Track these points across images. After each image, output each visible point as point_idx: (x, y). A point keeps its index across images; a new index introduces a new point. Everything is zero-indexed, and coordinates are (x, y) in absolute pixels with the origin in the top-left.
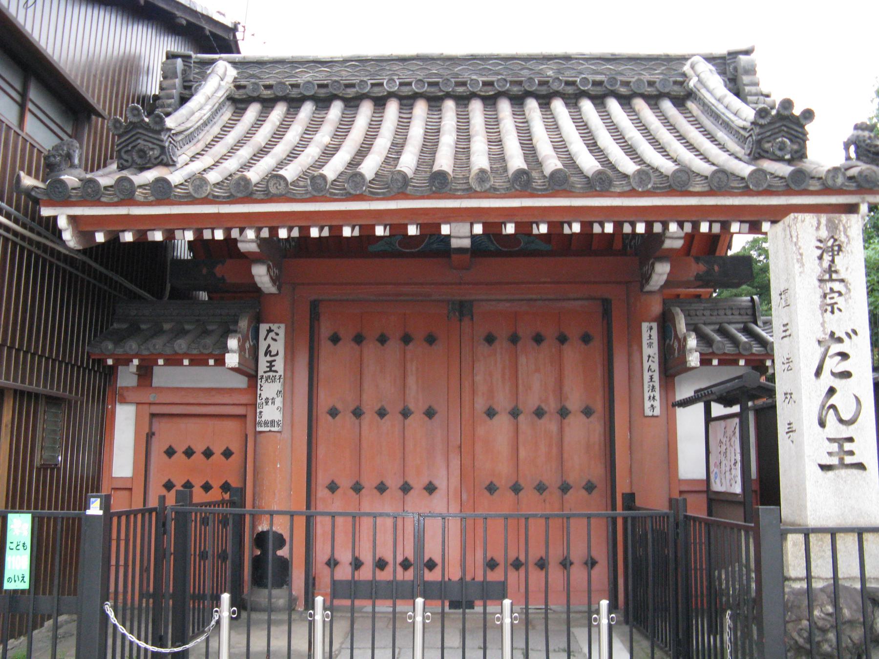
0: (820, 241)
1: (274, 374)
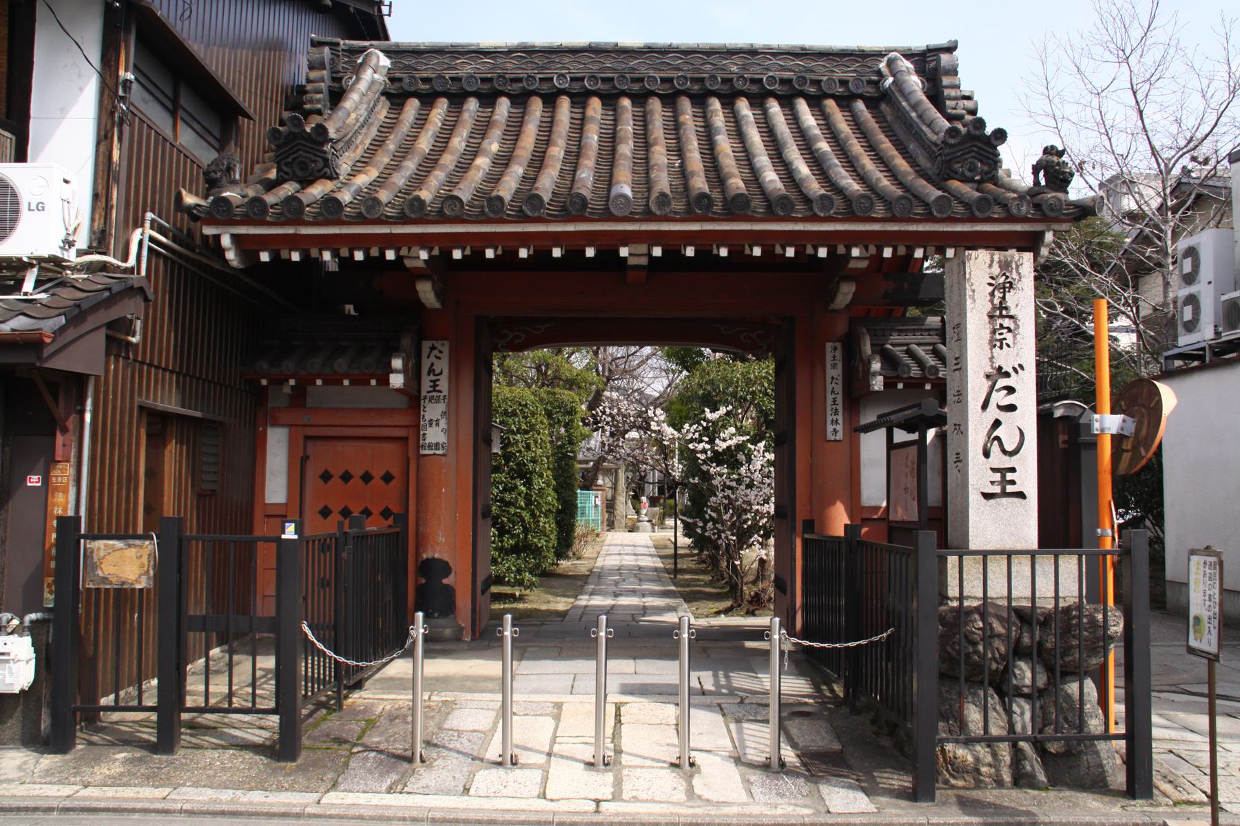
0: (992, 278)
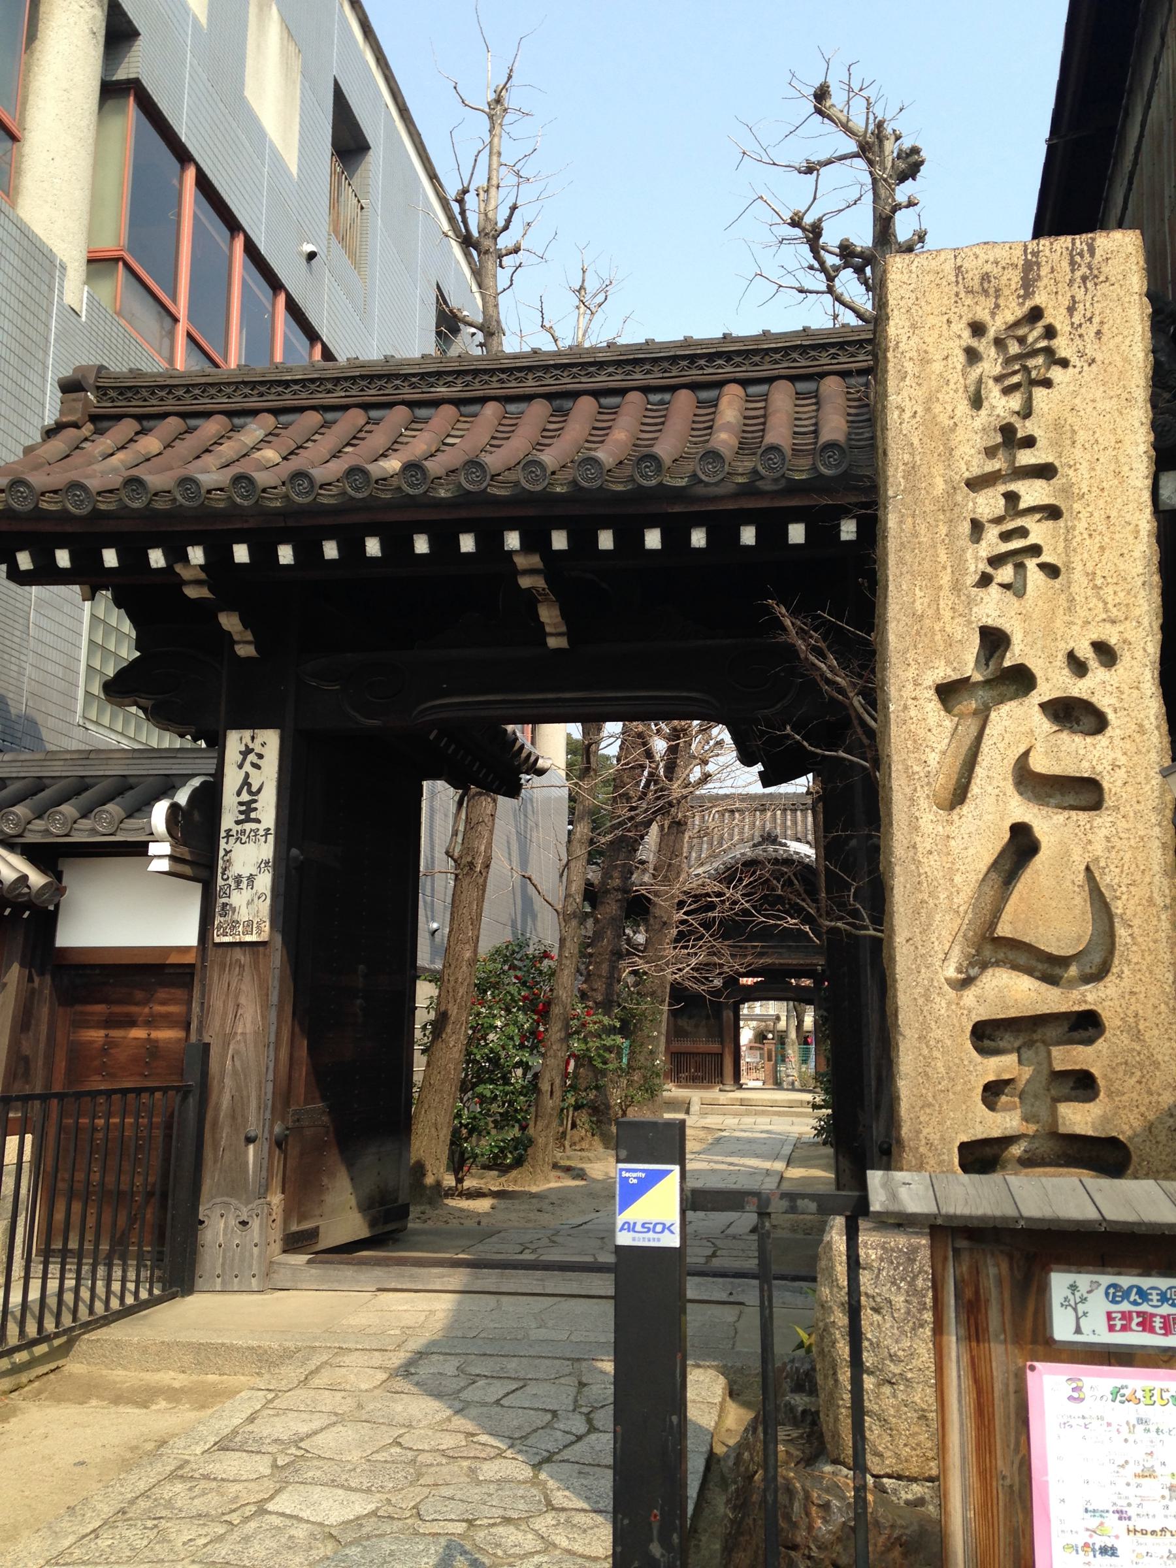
1: (254, 826)
